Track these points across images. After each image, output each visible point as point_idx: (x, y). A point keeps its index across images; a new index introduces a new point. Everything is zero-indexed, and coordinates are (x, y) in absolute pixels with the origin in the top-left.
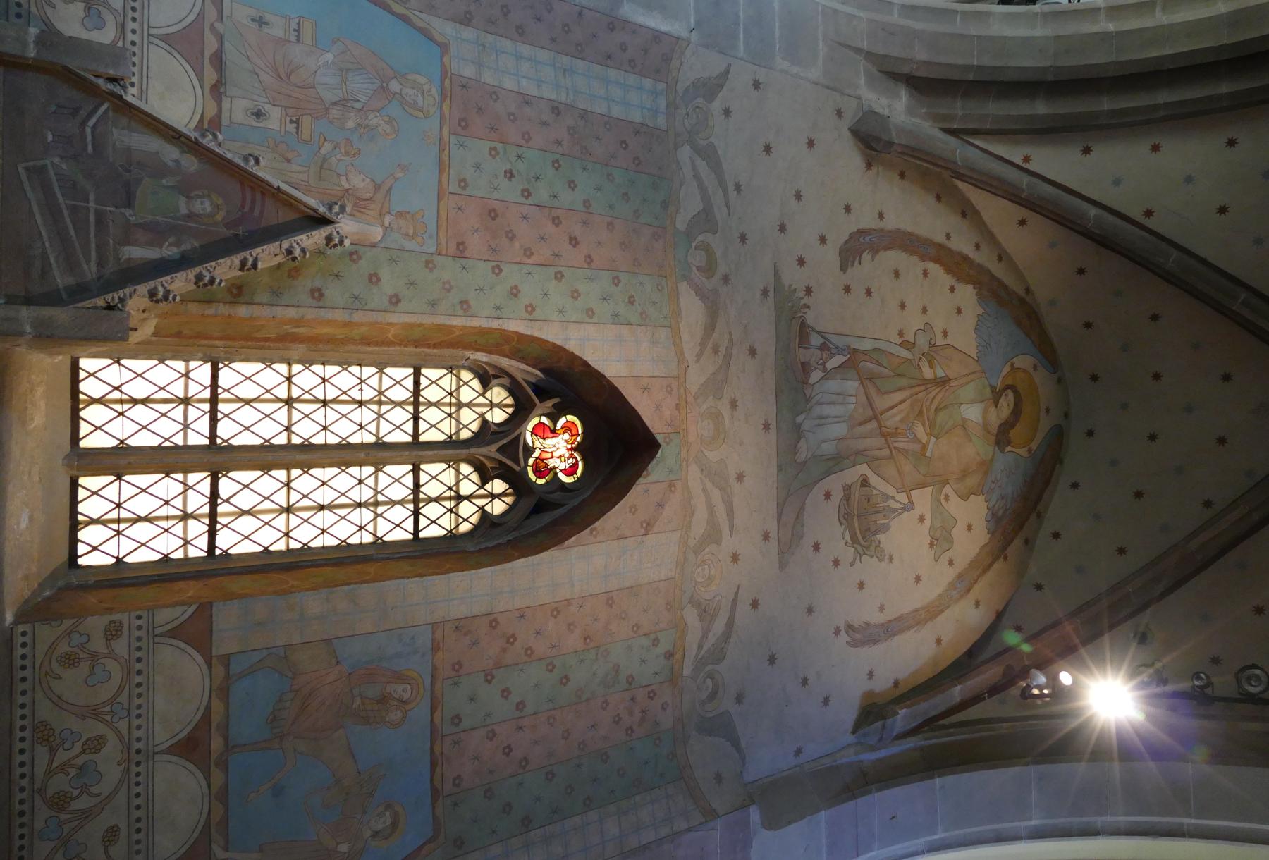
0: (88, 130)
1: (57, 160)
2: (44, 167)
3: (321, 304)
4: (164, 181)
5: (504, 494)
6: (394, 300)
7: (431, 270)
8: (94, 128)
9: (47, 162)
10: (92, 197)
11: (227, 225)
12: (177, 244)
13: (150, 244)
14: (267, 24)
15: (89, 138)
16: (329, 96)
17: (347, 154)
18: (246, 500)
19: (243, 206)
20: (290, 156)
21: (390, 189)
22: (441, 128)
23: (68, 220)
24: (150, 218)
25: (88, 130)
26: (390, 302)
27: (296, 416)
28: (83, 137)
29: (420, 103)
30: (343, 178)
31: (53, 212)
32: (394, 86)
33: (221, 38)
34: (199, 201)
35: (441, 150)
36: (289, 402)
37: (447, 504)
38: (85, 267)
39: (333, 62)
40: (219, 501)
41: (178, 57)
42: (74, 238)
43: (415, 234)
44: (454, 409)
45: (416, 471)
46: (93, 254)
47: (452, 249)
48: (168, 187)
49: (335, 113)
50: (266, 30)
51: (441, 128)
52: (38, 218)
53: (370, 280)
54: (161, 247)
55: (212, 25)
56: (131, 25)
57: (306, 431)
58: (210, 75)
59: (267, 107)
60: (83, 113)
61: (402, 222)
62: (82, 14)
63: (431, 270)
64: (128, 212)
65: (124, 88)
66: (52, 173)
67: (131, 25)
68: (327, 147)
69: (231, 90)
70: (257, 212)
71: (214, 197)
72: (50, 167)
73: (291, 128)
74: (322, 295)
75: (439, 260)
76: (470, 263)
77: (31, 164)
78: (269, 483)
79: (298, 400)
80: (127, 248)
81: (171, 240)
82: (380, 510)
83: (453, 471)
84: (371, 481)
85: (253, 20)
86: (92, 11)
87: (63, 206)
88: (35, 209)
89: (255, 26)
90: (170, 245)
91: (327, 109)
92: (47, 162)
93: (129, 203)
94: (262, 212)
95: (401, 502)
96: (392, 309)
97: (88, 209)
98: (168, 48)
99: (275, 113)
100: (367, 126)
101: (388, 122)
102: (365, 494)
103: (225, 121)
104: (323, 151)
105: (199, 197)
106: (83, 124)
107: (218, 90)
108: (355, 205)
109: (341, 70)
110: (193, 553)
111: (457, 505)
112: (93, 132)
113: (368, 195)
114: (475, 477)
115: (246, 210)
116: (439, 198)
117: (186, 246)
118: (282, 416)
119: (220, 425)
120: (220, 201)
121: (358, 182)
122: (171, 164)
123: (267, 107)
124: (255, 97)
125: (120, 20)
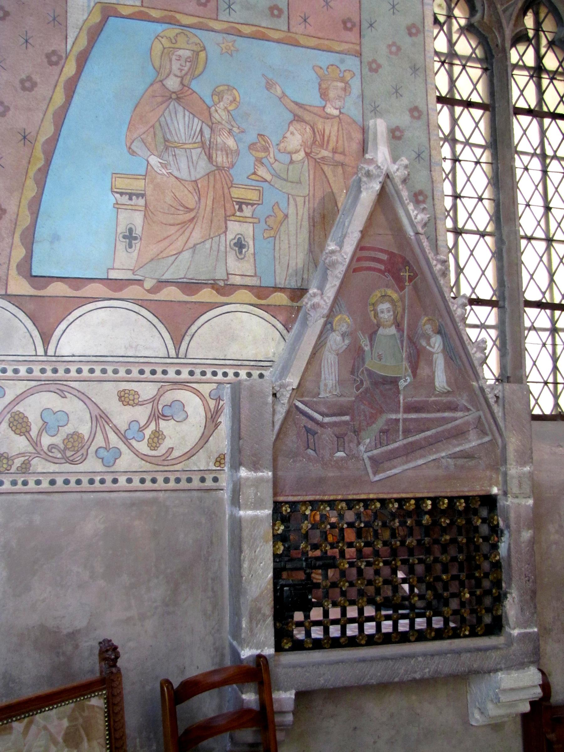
0: (327, 420)
1: (362, 448)
2: (370, 458)
3: (429, 194)
4: (367, 349)
5: (536, 15)
6: (416, 114)
7: (379, 66)
8: (323, 414)
9: (365, 456)
10: (394, 416)
11: (402, 288)
12: (428, 338)
13: (431, 363)
14: (131, 230)
15: (334, 419)
16: (203, 166)
17: (266, 149)
18: (542, 277)
19: (379, 271)
20: (280, 216)
21: (296, 104)
22: (213, 30)
23: (418, 437)
24: (405, 364)
25: (327, 420)
26: (419, 118)
27: (470, 226)
28: (334, 424)
29: (188, 53)
30: (295, 157)
31: (410, 451)
32: (173, 83)
33: (162, 284)
34: (381, 315)
35: (240, 34)
36: (549, 241)
37: (545, 82)
38: (458, 422)
39: (159, 156)
40: (544, 301)
41: (193, 328)
42: (433, 431)
43: (342, 80)
44: (457, 62)
45: (518, 111)
46: (446, 414)
47: (352, 36)
48: (372, 346)
49: (220, 158)
50: (138, 231)
51: (213, 30)
52: (420, 462)
53: (399, 138)
54: (431, 354)
55: (148, 291)
56: (171, 375)
57: (482, 218)
58: (206, 295)
59: (230, 236)
60: (310, 425)
61: (332, 94)
62: (172, 422)
63: (379, 66)
64: (402, 384)
65: (282, 386)
66: (375, 452)
67: (171, 375)
68: (262, 172)
69: (220, 274)
70: (385, 257)
71: (373, 300)
72: (370, 454)
73: (247, 211)
74: (421, 193)
75: (367, 56)
76: (365, 16)
77: (370, 470)
78: (530, 256)
79: (547, 231)
80: (437, 384)
81: (424, 343)
82: (549, 152)
83: (515, 72)
84: (526, 159)
85: (131, 247)
86: (167, 412)
87: (405, 442)
88: (411, 465)
89: (137, 244)
90: (429, 344)
91: (219, 168)
92: (365, 456)
93: (394, 381)
94: (382, 251)
95: (543, 133)
96: (424, 117)
97: (405, 420)
98: (187, 338)
99: (234, 229)
100: (229, 122)
101: (221, 100)
102: (536, 164)
103: (254, 282)
104: (268, 177)
105: (376, 315)
106: (321, 425)
107: (225, 289)
108: (322, 146)
109: (167, 148)
110: (492, 320)
111: (548, 72)
112: (327, 415)
113: (308, 129)
114: (521, 48)
115: (383, 267)
116: (296, 44)
117: (428, 328)
118: (472, 239)
119: (481, 297)
120: (378, 294)
121: (295, 140)
122: (347, 342)
123: (230, 236)
124: (222, 248)
125: (168, 386)
